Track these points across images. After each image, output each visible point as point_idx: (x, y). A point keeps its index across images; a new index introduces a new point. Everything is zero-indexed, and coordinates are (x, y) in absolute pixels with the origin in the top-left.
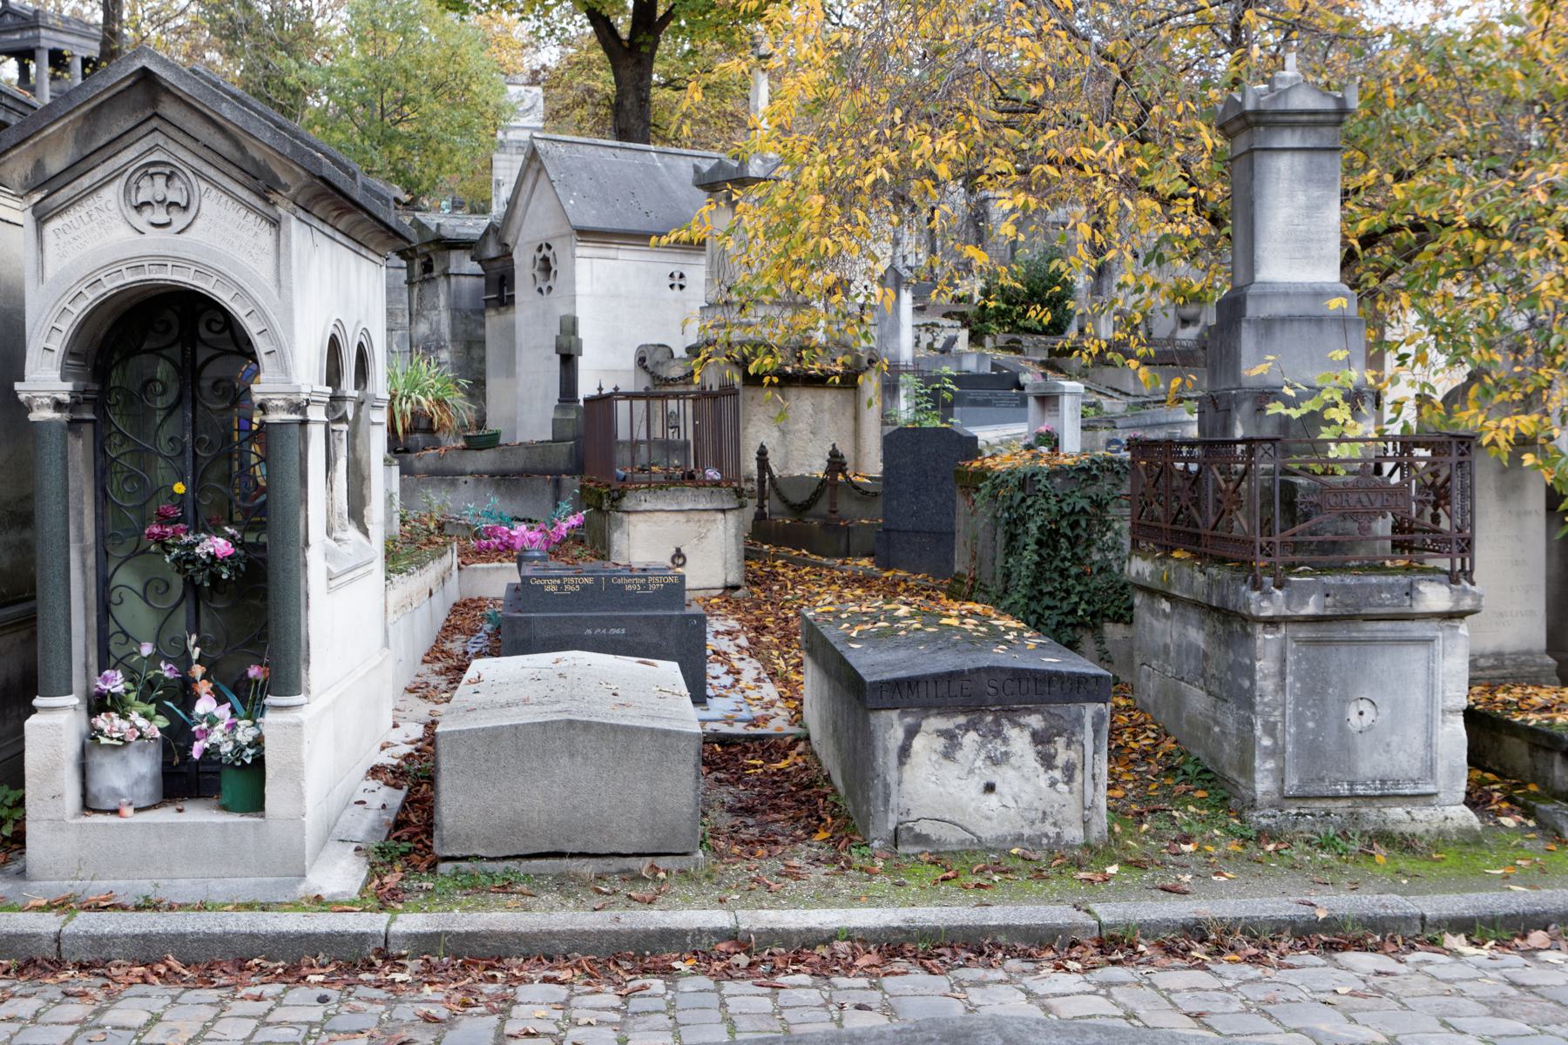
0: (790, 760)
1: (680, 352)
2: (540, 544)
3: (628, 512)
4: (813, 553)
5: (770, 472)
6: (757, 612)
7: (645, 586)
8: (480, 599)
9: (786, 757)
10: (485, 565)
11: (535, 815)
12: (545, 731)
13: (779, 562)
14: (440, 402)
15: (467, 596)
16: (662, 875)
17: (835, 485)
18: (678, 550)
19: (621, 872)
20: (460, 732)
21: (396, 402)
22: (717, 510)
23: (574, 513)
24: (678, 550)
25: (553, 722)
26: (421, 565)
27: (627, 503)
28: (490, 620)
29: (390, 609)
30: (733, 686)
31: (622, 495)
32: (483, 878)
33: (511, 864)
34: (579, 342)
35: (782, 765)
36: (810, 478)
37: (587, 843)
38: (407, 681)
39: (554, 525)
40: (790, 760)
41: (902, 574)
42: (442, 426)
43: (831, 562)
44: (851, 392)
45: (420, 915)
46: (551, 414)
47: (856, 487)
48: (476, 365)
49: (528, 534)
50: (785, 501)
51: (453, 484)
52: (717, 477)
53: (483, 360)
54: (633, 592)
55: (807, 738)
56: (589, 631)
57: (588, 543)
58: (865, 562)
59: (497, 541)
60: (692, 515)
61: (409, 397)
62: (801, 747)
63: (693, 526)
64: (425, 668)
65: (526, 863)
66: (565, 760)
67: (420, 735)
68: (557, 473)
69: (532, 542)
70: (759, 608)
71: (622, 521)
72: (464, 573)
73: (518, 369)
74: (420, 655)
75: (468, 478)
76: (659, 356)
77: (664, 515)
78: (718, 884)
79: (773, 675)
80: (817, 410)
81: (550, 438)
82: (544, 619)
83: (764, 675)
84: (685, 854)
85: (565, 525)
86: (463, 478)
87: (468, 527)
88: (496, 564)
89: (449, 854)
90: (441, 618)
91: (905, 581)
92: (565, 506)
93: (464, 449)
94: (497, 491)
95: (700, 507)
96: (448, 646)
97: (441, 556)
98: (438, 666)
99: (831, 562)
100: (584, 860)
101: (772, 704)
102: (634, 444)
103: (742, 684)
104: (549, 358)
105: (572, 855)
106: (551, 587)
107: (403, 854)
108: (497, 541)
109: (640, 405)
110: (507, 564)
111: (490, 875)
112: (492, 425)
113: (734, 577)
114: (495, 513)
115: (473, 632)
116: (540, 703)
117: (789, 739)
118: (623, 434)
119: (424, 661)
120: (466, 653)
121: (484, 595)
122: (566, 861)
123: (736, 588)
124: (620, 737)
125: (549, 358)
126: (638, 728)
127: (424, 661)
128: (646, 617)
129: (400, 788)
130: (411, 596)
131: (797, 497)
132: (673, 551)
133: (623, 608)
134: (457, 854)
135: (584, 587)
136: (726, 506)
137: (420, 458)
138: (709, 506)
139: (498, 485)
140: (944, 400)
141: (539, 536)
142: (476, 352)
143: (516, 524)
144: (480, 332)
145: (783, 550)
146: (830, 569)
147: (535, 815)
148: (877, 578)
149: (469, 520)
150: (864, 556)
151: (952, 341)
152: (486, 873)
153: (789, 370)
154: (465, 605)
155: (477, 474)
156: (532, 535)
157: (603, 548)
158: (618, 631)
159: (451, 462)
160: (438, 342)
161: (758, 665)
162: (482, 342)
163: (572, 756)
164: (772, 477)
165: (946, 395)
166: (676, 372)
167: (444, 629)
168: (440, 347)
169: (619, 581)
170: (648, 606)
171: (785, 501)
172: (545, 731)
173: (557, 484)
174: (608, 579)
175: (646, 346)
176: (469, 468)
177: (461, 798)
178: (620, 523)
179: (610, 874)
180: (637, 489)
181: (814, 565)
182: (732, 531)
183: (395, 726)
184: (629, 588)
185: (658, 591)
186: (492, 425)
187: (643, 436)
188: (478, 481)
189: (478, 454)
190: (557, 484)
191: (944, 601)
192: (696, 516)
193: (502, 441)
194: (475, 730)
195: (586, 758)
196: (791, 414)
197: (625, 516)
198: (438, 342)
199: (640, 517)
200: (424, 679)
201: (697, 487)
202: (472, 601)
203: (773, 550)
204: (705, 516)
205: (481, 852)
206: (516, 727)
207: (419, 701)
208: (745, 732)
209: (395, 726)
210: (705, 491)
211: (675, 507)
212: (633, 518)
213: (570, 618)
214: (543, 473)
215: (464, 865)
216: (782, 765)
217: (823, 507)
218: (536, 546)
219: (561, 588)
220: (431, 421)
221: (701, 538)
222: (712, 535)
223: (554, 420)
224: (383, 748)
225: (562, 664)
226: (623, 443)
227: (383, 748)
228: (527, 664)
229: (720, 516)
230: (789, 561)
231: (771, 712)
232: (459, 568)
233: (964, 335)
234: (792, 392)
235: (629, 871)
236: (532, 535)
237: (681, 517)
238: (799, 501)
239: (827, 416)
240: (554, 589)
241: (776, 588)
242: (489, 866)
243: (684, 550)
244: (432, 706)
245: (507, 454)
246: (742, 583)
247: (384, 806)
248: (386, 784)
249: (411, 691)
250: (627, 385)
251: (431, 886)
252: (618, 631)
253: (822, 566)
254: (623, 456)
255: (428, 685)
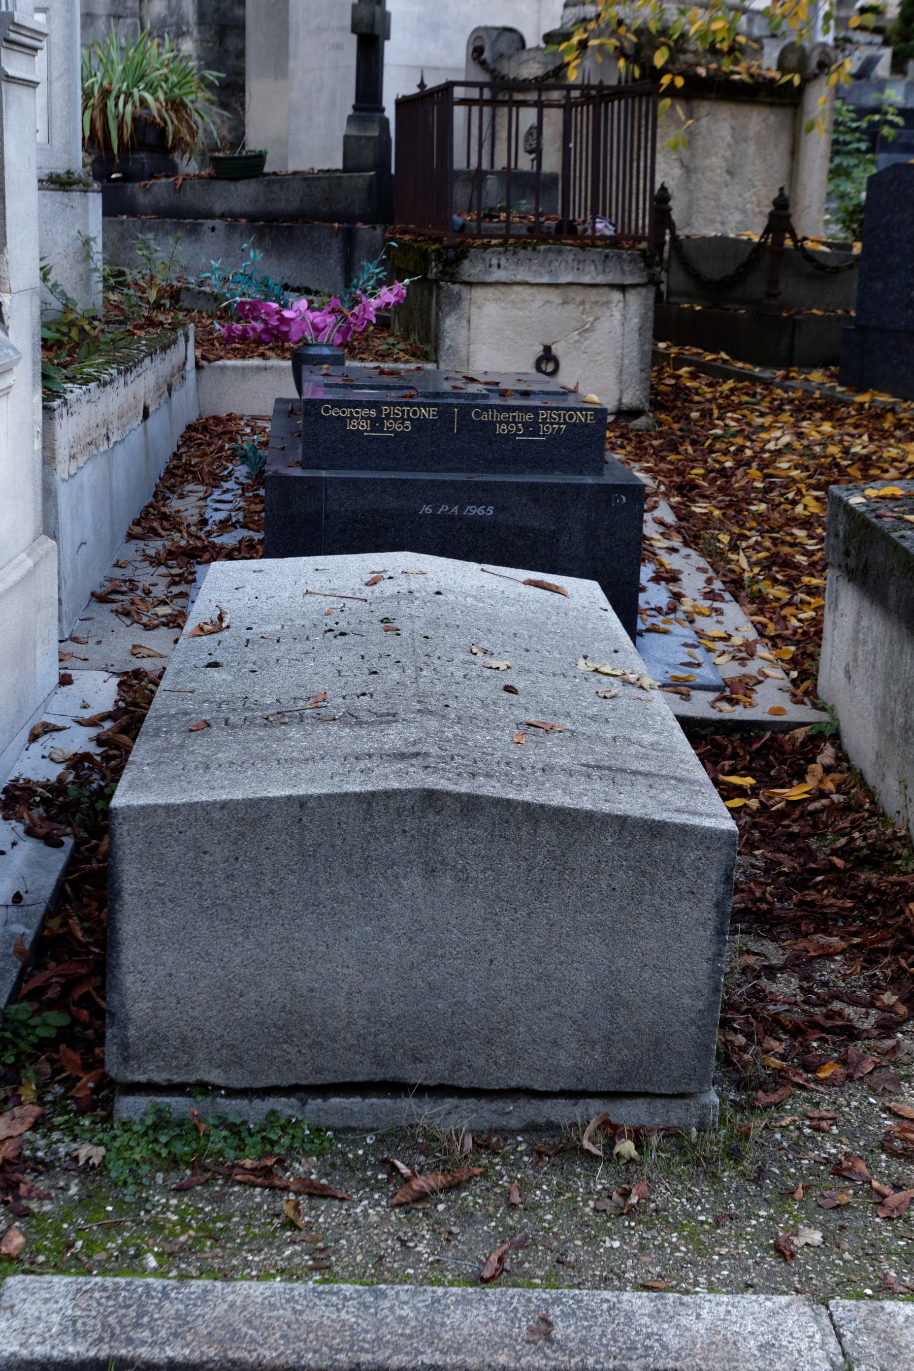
0: (811, 784)
1: (533, 40)
2: (331, 334)
3: (470, 284)
4: (736, 358)
5: (672, 226)
6: (672, 457)
7: (532, 428)
8: (231, 418)
9: (800, 775)
10: (239, 363)
11: (341, 1001)
12: (368, 816)
13: (684, 371)
14: (176, 105)
15: (209, 412)
16: (627, 1147)
17: (777, 249)
18: (547, 349)
19: (531, 1128)
20: (169, 809)
21: (111, 103)
22: (613, 286)
23: (388, 282)
24: (547, 349)
25: (389, 794)
26: (128, 366)
27: (470, 269)
28: (244, 459)
29: (62, 453)
30: (673, 610)
31: (462, 255)
32: (218, 1140)
33: (284, 1106)
34: (386, 17)
35: (796, 793)
36: (737, 242)
37: (457, 1065)
38: (96, 581)
39: (356, 302)
40: (811, 784)
41: (884, 398)
42: (179, 142)
43: (767, 374)
44: (789, 112)
45: (60, 1282)
46: (341, 129)
47: (809, 256)
48: (231, 62)
49: (310, 316)
50: (693, 274)
51: (194, 231)
52: (610, 231)
53: (241, 54)
54: (510, 437)
55: (836, 738)
56: (427, 509)
57: (397, 329)
58: (817, 376)
59: (259, 326)
60: (572, 292)
61: (129, 95)
62: (827, 755)
63: (572, 312)
64: (131, 551)
65: (315, 1103)
66: (412, 883)
67: (109, 707)
68: (351, 219)
69: (317, 329)
70: (675, 450)
71: (459, 298)
72: (206, 373)
73: (292, 64)
74: (125, 524)
75: (217, 223)
76: (504, 45)
77: (529, 290)
78: (758, 1180)
79: (736, 585)
80: (739, 137)
81: (339, 165)
82: (344, 482)
83: (717, 585)
84: (682, 1096)
85: (374, 303)
86: (210, 223)
87: (216, 298)
88: (256, 362)
89: (142, 1078)
90: (165, 449)
91: (893, 410)
92: (371, 270)
93: (211, 177)
94: (258, 244)
95: (587, 279)
96: (175, 504)
97: (165, 348)
98: (155, 546)
99: (767, 374)
100: (449, 1102)
101: (747, 652)
102: (477, 177)
103: (687, 605)
104: (338, 47)
105: (422, 1091)
106: (359, 424)
107: (43, 1045)
108: (259, 326)
109: (487, 110)
110: (274, 362)
111: (235, 1129)
112: (254, 141)
113: (633, 397)
114: (257, 277)
115: (215, 480)
116: (352, 719)
117: (800, 734)
118: (459, 162)
119: (131, 536)
120: (204, 522)
121: (237, 411)
122: (408, 1104)
123: (634, 413)
124: (547, 834)
125: (338, 47)
126: (589, 816)
127: (131, 536)
128: (533, 486)
129: (58, 844)
130: (106, 423)
131: (712, 270)
132: (539, 350)
133: (491, 466)
134: (160, 1078)
135: (420, 425)
136: (628, 280)
137: (146, 190)
138: (599, 279)
139: (261, 236)
140: (885, 139)
141: (330, 320)
142: (231, 42)
143: (291, 297)
144: (238, 12)
145: (691, 351)
146: (768, 384)
147: (341, 1001)
148: (847, 404)
149: (214, 286)
150: (814, 366)
151: (870, 64)
152: (223, 1123)
153: (702, 71)
154: (205, 428)
155: (227, 215)
156: (317, 317)
157: (426, 339)
158: (480, 511)
159: (192, 197)
160: (178, 26)
161: (703, 563)
162: (240, 27)
163: (431, 872)
164: (674, 238)
165: (886, 131)
166: (531, 70)
167: (169, 472)
168: (180, 34)
169: (485, 417)
170: (537, 465)
171: (693, 274)
172: (368, 816)
173: (349, 239)
174: (465, 410)
175: (486, 29)
176: (219, 207)
177: (169, 958)
178: (456, 302)
179: (507, 1133)
180: (486, 247)
181: (740, 376)
182: (635, 321)
183: (65, 680)
184: (502, 429)
185: (554, 438)
186: (254, 141)
187: (485, 166)
188: (231, 228)
189: (232, 186)
190: (349, 239)
191: (140, 236)
192: (578, 295)
193: (267, 169)
194: (206, 807)
195: (464, 877)
196: (700, 142)
197: (465, 290)
198: (178, 26)
199: (490, 292)
200: (128, 573)
201: (583, 247)
202: (217, 420)
203: (674, 350)
204: (593, 294)
205: (215, 1077)
206: (302, 802)
207: (115, 622)
208: (714, 715)
209: (65, 680)
210: (595, 254)
211: (545, 279)
212: (478, 293)
213: (393, 482)
214: (330, 218)
215: (177, 1104)
216: (796, 793)
217: (757, 287)
218: (324, 337)
219: (377, 423)
220: (163, 132)
221: (584, 331)
222: (604, 326)
223: (347, 138)
224: (34, 737)
225: (386, 588)
226: (460, 172)
227: (34, 737)
228: (318, 582)
229: (617, 296)
230: (700, 369)
231: (753, 667)
232: (198, 367)
233: (887, 54)
234: (704, 108)
235: (551, 1127)
236: (317, 317)
237: (555, 296)
238: (717, 276)
239: (752, 149)
240: (364, 426)
241: (695, 415)
242: (233, 1108)
243: (556, 350)
244: (136, 635)
245: (276, 188)
246: (647, 407)
247: (17, 898)
248: (30, 832)
249: (101, 598)
250: (461, 78)
251: (97, 1154)
252: (480, 511)
253: (754, 379)
254: (461, 194)
255: (132, 584)
